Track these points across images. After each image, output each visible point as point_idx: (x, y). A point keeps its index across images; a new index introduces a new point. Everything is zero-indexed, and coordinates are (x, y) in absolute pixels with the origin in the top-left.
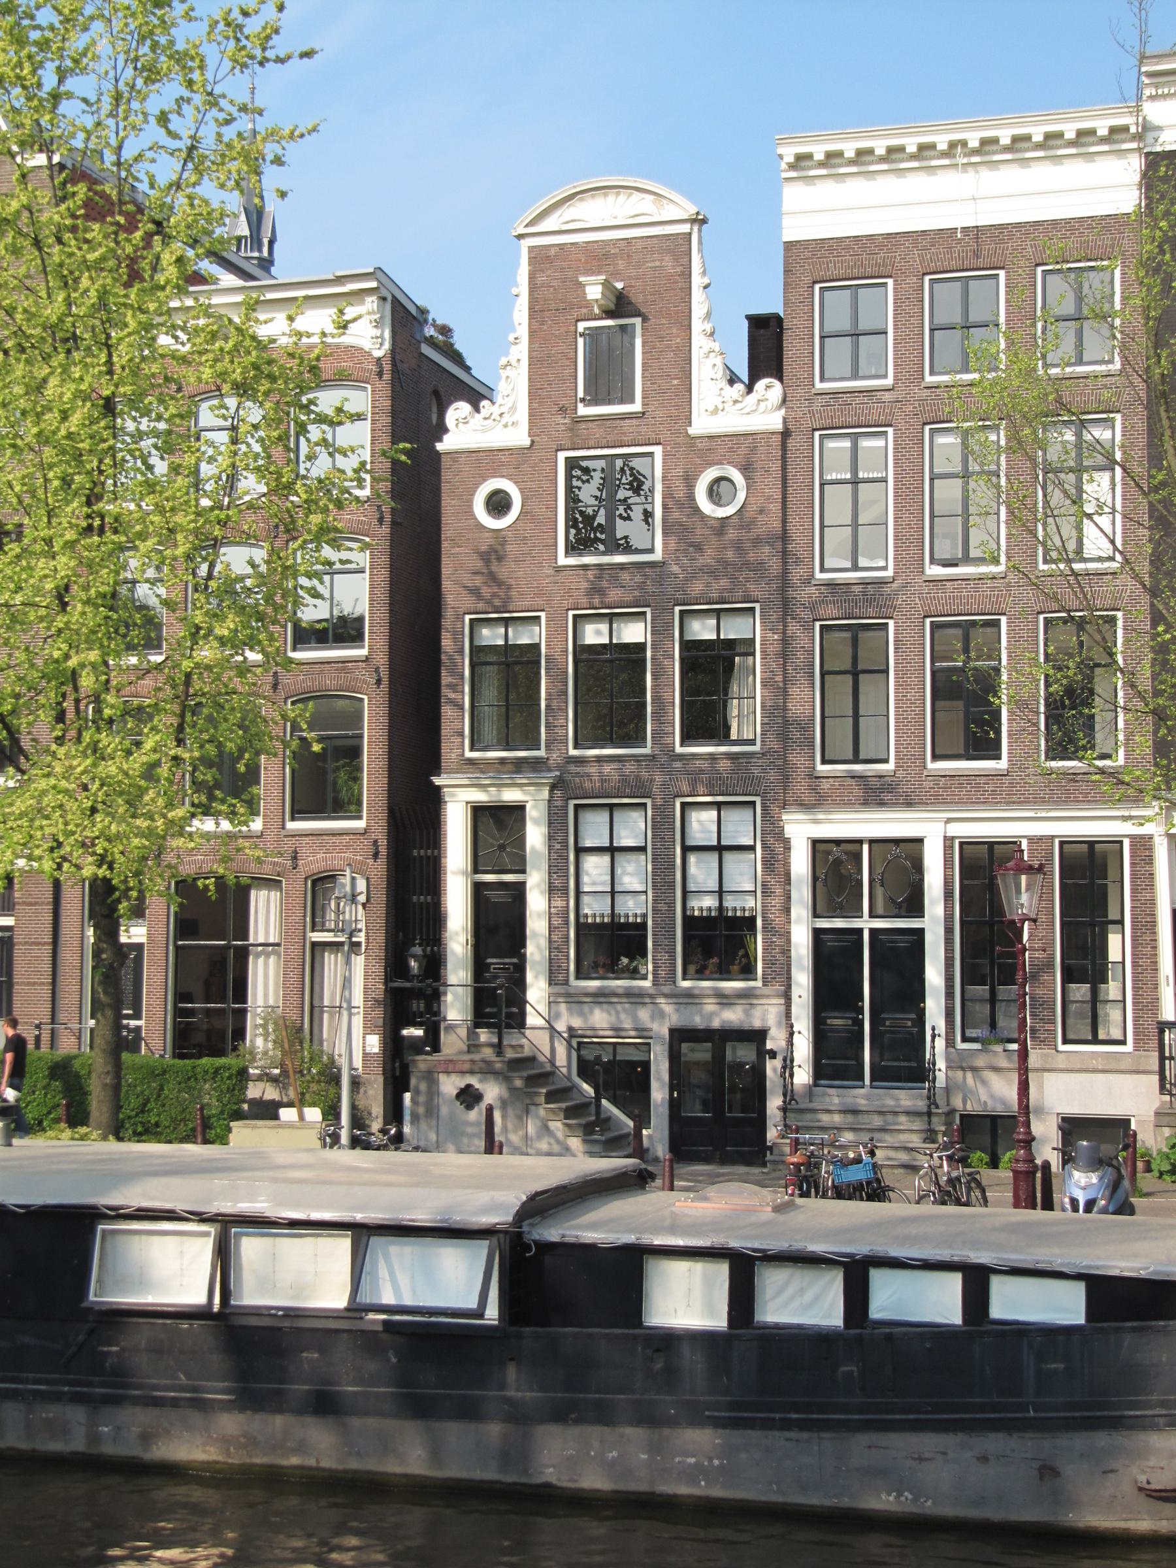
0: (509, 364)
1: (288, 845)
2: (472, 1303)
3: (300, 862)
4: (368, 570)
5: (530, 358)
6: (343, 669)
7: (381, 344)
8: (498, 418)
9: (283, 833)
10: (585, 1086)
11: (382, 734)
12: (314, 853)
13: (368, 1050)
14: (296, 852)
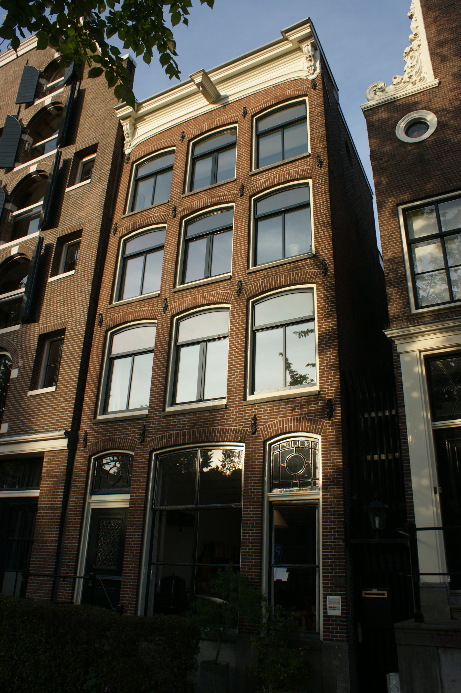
0: (412, 50)
1: (250, 412)
2: (311, 314)
3: (259, 428)
4: (318, 365)
5: (428, 39)
6: (294, 267)
7: (315, 70)
8: (408, 80)
9: (244, 403)
10: (367, 394)
11: (143, 582)
12: (272, 418)
13: (330, 612)
14: (255, 419)
